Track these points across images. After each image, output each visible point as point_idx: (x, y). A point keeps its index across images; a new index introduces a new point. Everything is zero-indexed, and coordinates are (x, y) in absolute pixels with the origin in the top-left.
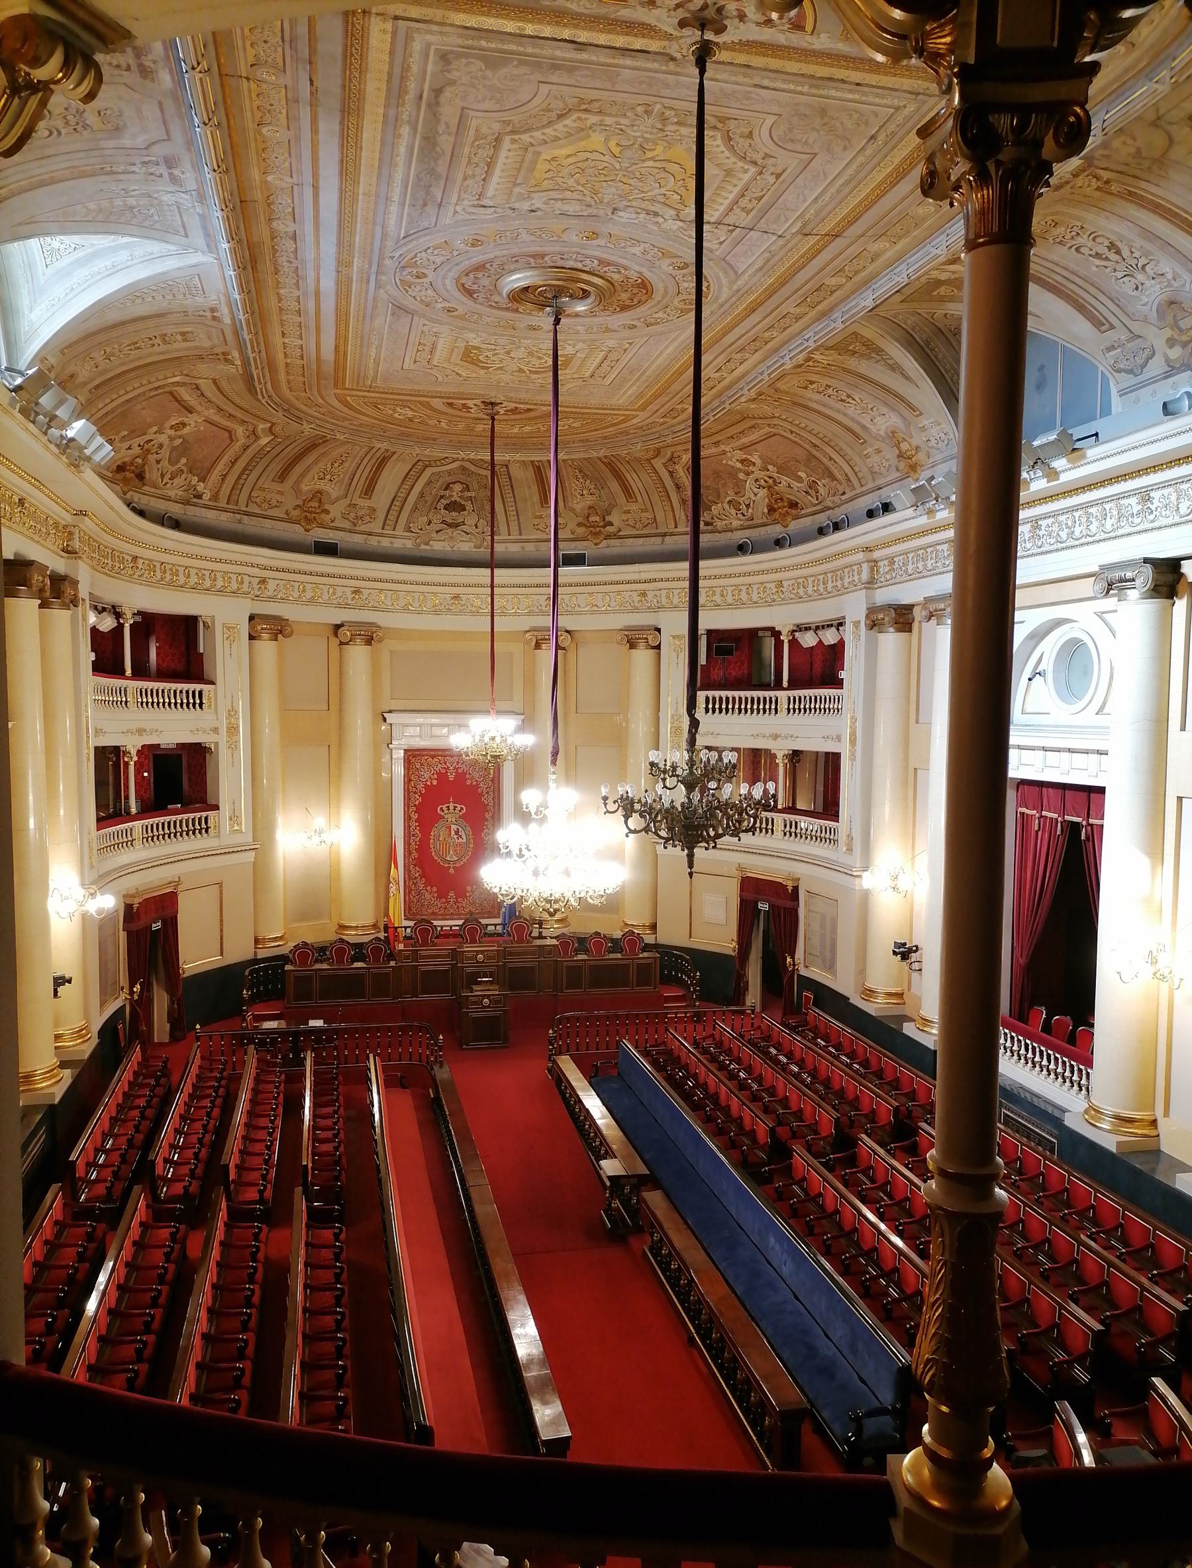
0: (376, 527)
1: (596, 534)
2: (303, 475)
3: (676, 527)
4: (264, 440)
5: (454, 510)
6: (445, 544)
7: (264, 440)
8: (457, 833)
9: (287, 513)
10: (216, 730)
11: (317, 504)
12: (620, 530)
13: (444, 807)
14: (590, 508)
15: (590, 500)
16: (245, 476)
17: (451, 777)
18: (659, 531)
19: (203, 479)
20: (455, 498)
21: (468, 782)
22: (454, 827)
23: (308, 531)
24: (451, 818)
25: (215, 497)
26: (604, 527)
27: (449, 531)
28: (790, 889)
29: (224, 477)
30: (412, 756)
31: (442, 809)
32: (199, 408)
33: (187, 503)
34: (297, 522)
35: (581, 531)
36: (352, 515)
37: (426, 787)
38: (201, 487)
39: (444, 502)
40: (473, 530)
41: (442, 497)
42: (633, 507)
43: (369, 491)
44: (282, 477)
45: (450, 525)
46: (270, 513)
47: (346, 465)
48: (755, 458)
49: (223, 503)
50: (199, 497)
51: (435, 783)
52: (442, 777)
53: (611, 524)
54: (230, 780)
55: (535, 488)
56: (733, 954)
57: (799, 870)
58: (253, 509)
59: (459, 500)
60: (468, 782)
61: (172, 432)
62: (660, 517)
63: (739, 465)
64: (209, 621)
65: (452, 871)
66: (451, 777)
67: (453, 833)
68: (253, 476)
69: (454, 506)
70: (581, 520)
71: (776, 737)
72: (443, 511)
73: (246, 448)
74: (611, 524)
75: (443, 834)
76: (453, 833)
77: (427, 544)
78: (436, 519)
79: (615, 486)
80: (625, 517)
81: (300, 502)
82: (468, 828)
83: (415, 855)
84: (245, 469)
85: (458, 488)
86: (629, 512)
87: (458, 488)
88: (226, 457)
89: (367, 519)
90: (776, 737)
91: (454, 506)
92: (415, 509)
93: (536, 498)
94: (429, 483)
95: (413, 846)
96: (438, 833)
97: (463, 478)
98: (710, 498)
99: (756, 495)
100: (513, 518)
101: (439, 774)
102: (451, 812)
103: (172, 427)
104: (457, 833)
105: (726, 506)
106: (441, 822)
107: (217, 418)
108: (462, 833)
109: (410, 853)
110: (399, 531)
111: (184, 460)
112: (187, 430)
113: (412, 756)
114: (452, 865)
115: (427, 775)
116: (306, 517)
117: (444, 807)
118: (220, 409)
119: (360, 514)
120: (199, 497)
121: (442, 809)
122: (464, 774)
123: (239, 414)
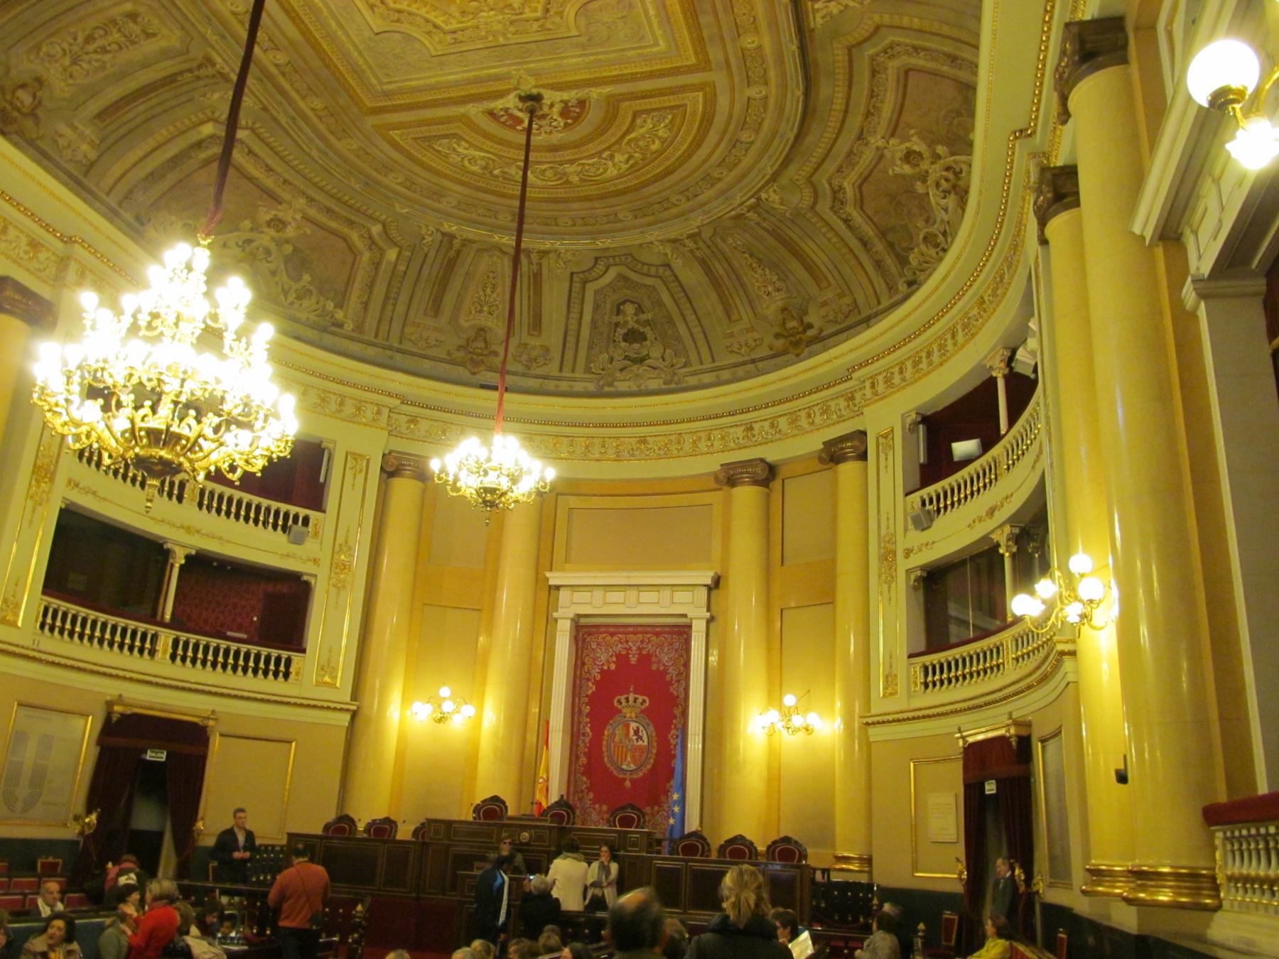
0: (553, 369)
1: (796, 344)
2: (457, 307)
3: (879, 303)
4: (392, 255)
5: (635, 341)
6: (631, 383)
7: (392, 255)
8: (637, 732)
9: (449, 354)
10: (315, 561)
11: (482, 345)
12: (821, 330)
13: (623, 698)
14: (784, 310)
15: (779, 300)
16: (389, 307)
17: (633, 660)
18: (864, 315)
19: (340, 305)
20: (632, 324)
21: (654, 667)
22: (633, 725)
23: (474, 374)
24: (629, 713)
25: (359, 328)
26: (804, 331)
27: (635, 368)
28: (1014, 742)
29: (366, 305)
30: (584, 632)
31: (620, 701)
32: (286, 196)
33: (324, 330)
34: (462, 364)
35: (780, 343)
36: (525, 357)
37: (602, 672)
38: (340, 315)
39: (621, 331)
40: (660, 364)
41: (617, 325)
42: (829, 294)
43: (536, 324)
44: (436, 307)
45: (634, 361)
46: (429, 352)
47: (499, 290)
48: (918, 145)
49: (369, 337)
50: (340, 326)
51: (613, 667)
52: (622, 659)
53: (810, 326)
54: (331, 625)
55: (713, 295)
56: (959, 889)
57: (1024, 707)
58: (407, 346)
59: (636, 326)
60: (654, 667)
61: (272, 232)
62: (861, 299)
63: (907, 169)
64: (331, 446)
65: (628, 784)
66: (633, 660)
67: (632, 732)
68: (401, 308)
69: (633, 336)
70: (778, 329)
71: (991, 512)
72: (623, 344)
73: (377, 265)
74: (810, 326)
75: (619, 732)
76: (632, 732)
77: (611, 385)
78: (618, 355)
79: (796, 267)
80: (823, 312)
81: (463, 342)
82: (651, 728)
83: (583, 760)
84: (387, 297)
85: (629, 309)
86: (824, 304)
87: (629, 309)
88: (359, 279)
89: (541, 361)
90: (188, 530)
91: (633, 336)
92: (590, 347)
93: (720, 310)
94: (597, 308)
95: (583, 748)
96: (614, 733)
97: (628, 293)
98: (904, 245)
99: (946, 210)
100: (701, 343)
101: (619, 656)
102: (631, 705)
103: (269, 224)
104: (637, 732)
105: (923, 247)
106: (617, 718)
107: (313, 212)
108: (644, 734)
109: (578, 758)
110: (579, 374)
111: (307, 277)
112: (290, 232)
113: (584, 632)
114: (628, 776)
115: (604, 658)
116: (472, 359)
117: (623, 701)
118: (311, 200)
119: (535, 354)
120: (340, 326)
121: (620, 701)
122: (649, 656)
123: (298, 181)
